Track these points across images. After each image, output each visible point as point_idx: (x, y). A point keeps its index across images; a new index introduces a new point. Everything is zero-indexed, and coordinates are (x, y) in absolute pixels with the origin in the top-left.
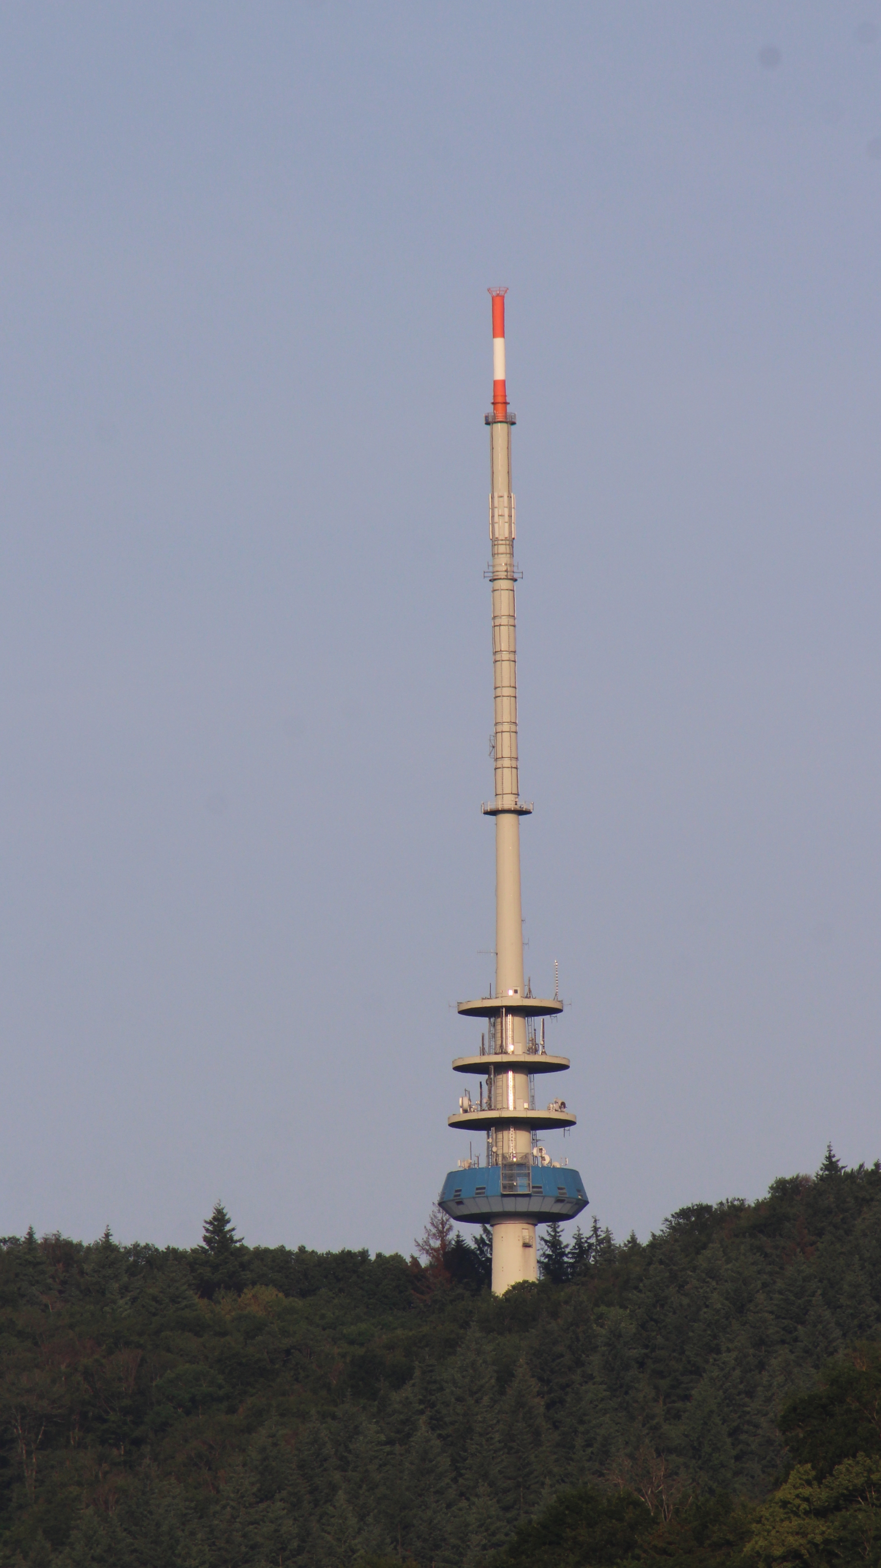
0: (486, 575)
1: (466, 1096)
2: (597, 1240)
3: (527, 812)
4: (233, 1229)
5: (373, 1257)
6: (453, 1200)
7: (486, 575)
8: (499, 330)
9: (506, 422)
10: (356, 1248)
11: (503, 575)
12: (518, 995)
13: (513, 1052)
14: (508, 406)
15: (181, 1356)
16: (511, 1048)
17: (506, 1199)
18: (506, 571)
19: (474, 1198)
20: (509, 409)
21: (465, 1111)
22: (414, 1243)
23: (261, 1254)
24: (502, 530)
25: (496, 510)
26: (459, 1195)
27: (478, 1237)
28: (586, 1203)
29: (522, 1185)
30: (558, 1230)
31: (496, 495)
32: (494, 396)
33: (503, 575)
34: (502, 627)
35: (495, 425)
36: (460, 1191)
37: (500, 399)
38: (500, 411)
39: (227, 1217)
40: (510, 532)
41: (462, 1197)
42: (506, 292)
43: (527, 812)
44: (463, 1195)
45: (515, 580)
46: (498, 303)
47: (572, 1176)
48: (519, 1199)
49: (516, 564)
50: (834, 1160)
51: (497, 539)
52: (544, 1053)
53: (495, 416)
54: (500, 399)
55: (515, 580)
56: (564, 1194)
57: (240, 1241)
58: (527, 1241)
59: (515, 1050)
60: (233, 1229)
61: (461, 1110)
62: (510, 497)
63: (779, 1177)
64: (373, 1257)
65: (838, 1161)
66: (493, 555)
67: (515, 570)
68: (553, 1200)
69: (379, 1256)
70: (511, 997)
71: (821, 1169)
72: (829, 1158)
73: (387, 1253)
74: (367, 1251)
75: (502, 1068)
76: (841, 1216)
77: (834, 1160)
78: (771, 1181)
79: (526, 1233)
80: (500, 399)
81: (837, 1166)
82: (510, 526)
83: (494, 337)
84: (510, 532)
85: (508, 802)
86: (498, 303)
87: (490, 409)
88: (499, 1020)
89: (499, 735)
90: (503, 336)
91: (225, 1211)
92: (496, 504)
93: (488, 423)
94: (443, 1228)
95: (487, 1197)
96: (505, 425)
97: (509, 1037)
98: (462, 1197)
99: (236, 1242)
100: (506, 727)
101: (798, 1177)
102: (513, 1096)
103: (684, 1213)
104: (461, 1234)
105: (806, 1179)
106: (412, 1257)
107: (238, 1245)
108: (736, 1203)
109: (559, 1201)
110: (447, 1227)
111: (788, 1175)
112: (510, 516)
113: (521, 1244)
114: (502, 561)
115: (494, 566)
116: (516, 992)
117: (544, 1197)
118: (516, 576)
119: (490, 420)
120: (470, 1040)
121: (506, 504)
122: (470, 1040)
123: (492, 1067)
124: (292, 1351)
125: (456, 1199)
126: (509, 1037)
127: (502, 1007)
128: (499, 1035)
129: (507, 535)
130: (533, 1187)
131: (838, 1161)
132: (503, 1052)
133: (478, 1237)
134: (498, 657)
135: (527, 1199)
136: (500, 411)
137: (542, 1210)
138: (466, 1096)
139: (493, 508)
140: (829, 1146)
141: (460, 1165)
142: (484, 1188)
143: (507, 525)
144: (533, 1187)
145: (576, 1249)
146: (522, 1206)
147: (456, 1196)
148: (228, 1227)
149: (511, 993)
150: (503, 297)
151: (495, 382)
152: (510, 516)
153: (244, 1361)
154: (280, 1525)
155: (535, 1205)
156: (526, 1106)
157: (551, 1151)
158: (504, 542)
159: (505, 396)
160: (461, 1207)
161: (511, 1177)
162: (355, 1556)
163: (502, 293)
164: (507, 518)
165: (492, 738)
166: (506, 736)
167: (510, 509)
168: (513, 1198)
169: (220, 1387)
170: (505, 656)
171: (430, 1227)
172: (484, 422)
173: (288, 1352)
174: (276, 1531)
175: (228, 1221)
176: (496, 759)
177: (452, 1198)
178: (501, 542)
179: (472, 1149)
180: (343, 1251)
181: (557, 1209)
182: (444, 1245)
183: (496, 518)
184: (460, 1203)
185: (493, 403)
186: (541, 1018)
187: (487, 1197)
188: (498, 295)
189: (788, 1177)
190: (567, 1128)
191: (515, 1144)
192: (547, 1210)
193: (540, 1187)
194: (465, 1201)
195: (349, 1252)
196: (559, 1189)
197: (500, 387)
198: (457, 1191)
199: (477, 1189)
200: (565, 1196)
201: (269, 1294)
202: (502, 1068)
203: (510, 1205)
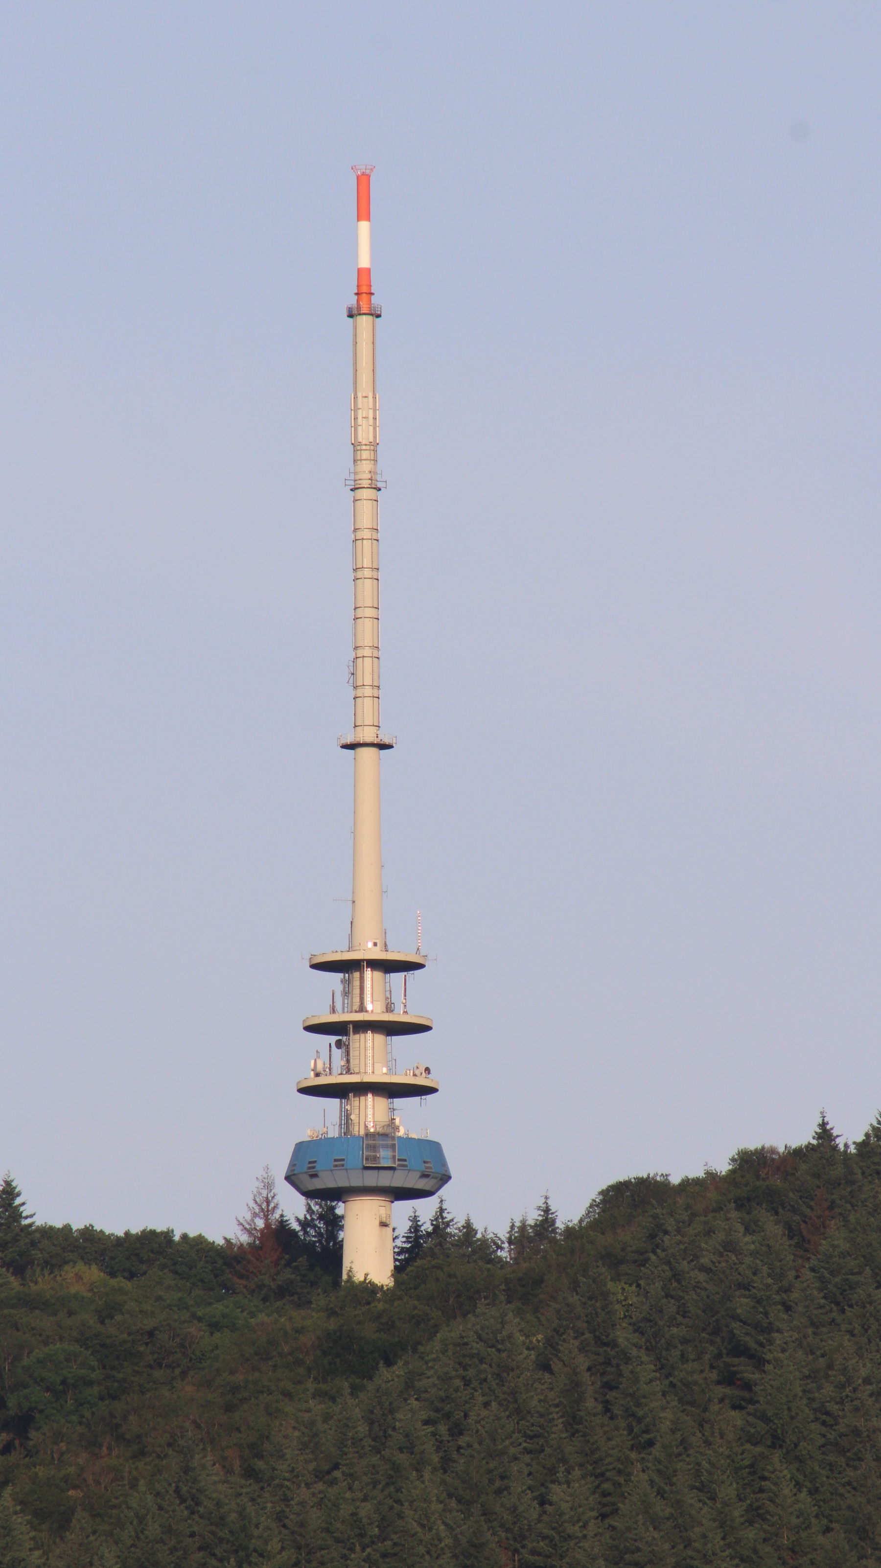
0: (348, 482)
1: (318, 1057)
3: (389, 747)
4: (23, 1204)
5: (177, 1238)
6: (306, 1173)
7: (348, 482)
8: (363, 212)
9: (372, 314)
10: (160, 1228)
11: (366, 483)
12: (378, 948)
13: (372, 1011)
14: (373, 297)
15: (34, 1335)
16: (369, 1007)
18: (371, 479)
19: (332, 1170)
21: (317, 1075)
22: (236, 1222)
23: (47, 1232)
24: (365, 435)
25: (360, 412)
26: (314, 1167)
27: (302, 1217)
28: (449, 1178)
29: (385, 1157)
31: (360, 395)
32: (358, 286)
33: (366, 483)
34: (365, 541)
35: (359, 318)
37: (364, 289)
38: (363, 305)
39: (17, 1190)
40: (375, 437)
41: (317, 1168)
42: (372, 170)
43: (389, 747)
44: (318, 1167)
45: (379, 490)
46: (363, 182)
47: (433, 1149)
48: (382, 1172)
49: (379, 472)
50: (828, 1127)
51: (360, 444)
52: (406, 1012)
53: (359, 307)
54: (364, 290)
55: (379, 490)
56: (430, 1168)
57: (31, 1216)
58: (384, 1220)
59: (374, 1010)
60: (23, 1204)
61: (312, 1074)
62: (374, 398)
63: (742, 1147)
64: (177, 1238)
65: (832, 1129)
66: (355, 461)
67: (379, 478)
68: (418, 1174)
69: (185, 1237)
70: (369, 951)
71: (814, 1138)
72: (823, 1125)
73: (192, 1234)
74: (173, 1231)
75: (362, 1027)
76: (849, 1189)
77: (828, 1127)
78: (733, 1152)
79: (383, 1211)
80: (364, 290)
81: (831, 1135)
82: (375, 429)
83: (359, 219)
84: (375, 437)
85: (368, 735)
86: (363, 182)
87: (353, 301)
88: (357, 975)
89: (360, 661)
90: (368, 219)
91: (14, 1184)
92: (360, 405)
93: (351, 316)
94: (268, 1205)
95: (346, 1170)
96: (370, 317)
97: (362, 996)
98: (317, 1168)
99: (26, 1218)
100: (367, 652)
101: (763, 1148)
102: (374, 1059)
104: (285, 1214)
105: (773, 1151)
106: (225, 1239)
107: (25, 1222)
108: (658, 1179)
109: (425, 1176)
110: (272, 1205)
111: (753, 1145)
112: (375, 419)
113: (378, 1223)
114: (365, 467)
115: (355, 473)
116: (375, 944)
117: (409, 1170)
118: (379, 485)
119: (355, 312)
120: (324, 996)
121: (371, 406)
122: (324, 996)
123: (351, 1026)
124: (157, 1332)
125: (307, 1170)
126: (362, 996)
127: (363, 960)
128: (357, 991)
129: (371, 440)
130: (399, 1160)
131: (832, 1129)
132: (362, 1009)
133: (302, 1217)
134: (359, 574)
135: (390, 1172)
136: (363, 305)
137: (416, 1187)
138: (318, 1057)
139: (356, 409)
140: (822, 1113)
141: (306, 1135)
142: (343, 1160)
143: (371, 428)
144: (399, 1160)
145: (411, 1232)
146: (385, 1180)
147: (309, 1168)
148: (17, 1201)
149: (370, 945)
150: (369, 176)
151: (359, 270)
152: (375, 419)
153: (108, 1341)
154: (358, 1508)
155: (398, 1180)
156: (385, 1070)
157: (411, 1119)
158: (368, 447)
159: (370, 286)
160: (315, 1180)
161: (374, 1148)
162: (442, 1545)
163: (368, 172)
164: (371, 421)
165: (351, 664)
166: (368, 661)
167: (375, 410)
168: (376, 1171)
169: (93, 1369)
170: (367, 573)
171: (252, 1204)
172: (345, 314)
173: (151, 1334)
174: (353, 1514)
175: (18, 1195)
176: (355, 688)
177: (305, 1170)
178: (364, 447)
181: (422, 1184)
182: (268, 1225)
184: (314, 1176)
185: (357, 294)
186: (402, 974)
187: (346, 1170)
188: (363, 174)
189: (752, 1148)
190: (423, 1097)
191: (371, 1112)
192: (400, 1185)
193: (405, 1160)
194: (320, 1174)
195: (153, 1233)
196: (425, 1162)
197: (364, 275)
198: (310, 1163)
199: (336, 1160)
200: (422, 1172)
201: (94, 1273)
202: (362, 1027)
203: (372, 1179)
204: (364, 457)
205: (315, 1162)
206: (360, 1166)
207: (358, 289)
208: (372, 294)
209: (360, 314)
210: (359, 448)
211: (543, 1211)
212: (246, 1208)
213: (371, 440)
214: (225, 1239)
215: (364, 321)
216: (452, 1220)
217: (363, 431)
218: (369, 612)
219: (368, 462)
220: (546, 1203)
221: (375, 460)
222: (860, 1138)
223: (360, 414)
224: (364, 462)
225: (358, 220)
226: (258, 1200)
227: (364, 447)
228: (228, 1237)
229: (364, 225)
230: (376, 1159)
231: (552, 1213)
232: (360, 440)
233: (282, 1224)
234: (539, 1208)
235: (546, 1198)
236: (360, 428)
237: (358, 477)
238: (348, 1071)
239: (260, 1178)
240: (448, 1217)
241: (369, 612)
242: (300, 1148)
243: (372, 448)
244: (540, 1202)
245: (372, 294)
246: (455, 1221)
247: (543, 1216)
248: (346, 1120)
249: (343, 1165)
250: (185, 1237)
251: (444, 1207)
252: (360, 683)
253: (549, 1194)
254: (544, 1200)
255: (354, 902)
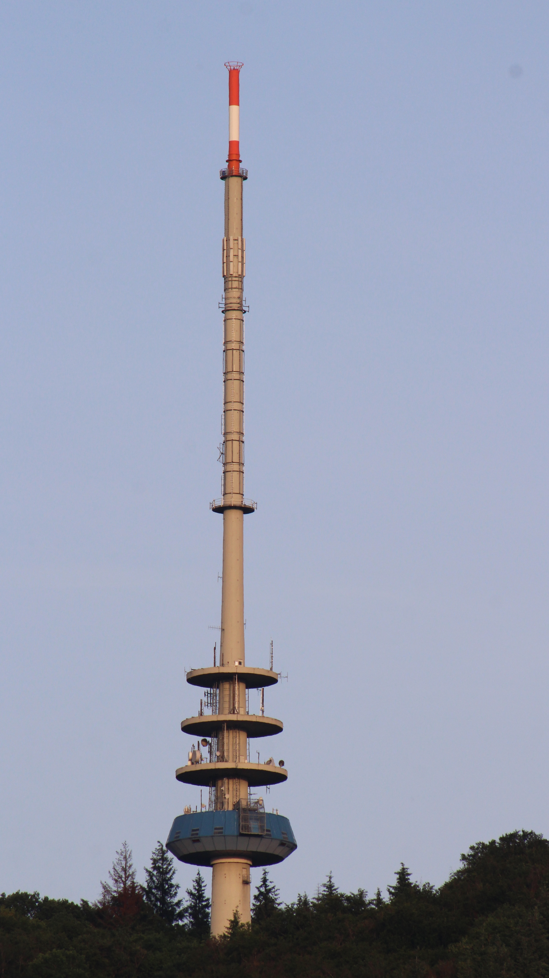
0: (221, 305)
2: (266, 890)
6: (190, 838)
7: (221, 305)
17: (241, 839)
20: (241, 165)
25: (232, 251)
26: (197, 834)
29: (254, 828)
30: (203, 885)
31: (231, 238)
36: (179, 833)
46: (234, 75)
54: (234, 158)
69: (46, 899)
80: (234, 158)
85: (234, 500)
86: (234, 75)
93: (223, 178)
95: (224, 836)
97: (228, 704)
103: (513, 837)
113: (241, 881)
121: (240, 247)
126: (228, 704)
127: (235, 674)
132: (233, 711)
135: (258, 840)
139: (228, 249)
146: (244, 845)
147: (193, 835)
158: (237, 279)
172: (219, 176)
178: (234, 279)
179: (199, 798)
180: (17, 893)
182: (125, 888)
183: (231, 258)
184: (197, 841)
196: (283, 834)
198: (193, 830)
200: (270, 843)
203: (231, 847)
204: (234, 286)
205: (198, 830)
206: (236, 833)
207: (229, 158)
208: (240, 161)
209: (232, 176)
210: (230, 279)
211: (327, 888)
212: (109, 875)
213: (240, 273)
214: (83, 900)
215: (234, 181)
216: (273, 888)
217: (234, 266)
218: (236, 406)
219: (237, 290)
220: (330, 881)
221: (242, 289)
222: (289, 903)
223: (232, 253)
224: (234, 290)
225: (230, 104)
226: (117, 869)
227: (234, 279)
228: (85, 900)
229: (234, 108)
230: (247, 828)
231: (335, 890)
232: (231, 273)
233: (133, 886)
234: (324, 885)
235: (330, 878)
236: (231, 264)
237: (229, 301)
238: (221, 759)
239: (120, 852)
240: (270, 886)
241: (236, 406)
242: (179, 822)
243: (240, 279)
244: (326, 881)
245: (240, 161)
246: (276, 888)
247: (328, 891)
248: (219, 800)
249: (222, 833)
250: (46, 899)
251: (267, 878)
252: (229, 460)
253: (332, 875)
254: (328, 880)
255: (223, 630)
